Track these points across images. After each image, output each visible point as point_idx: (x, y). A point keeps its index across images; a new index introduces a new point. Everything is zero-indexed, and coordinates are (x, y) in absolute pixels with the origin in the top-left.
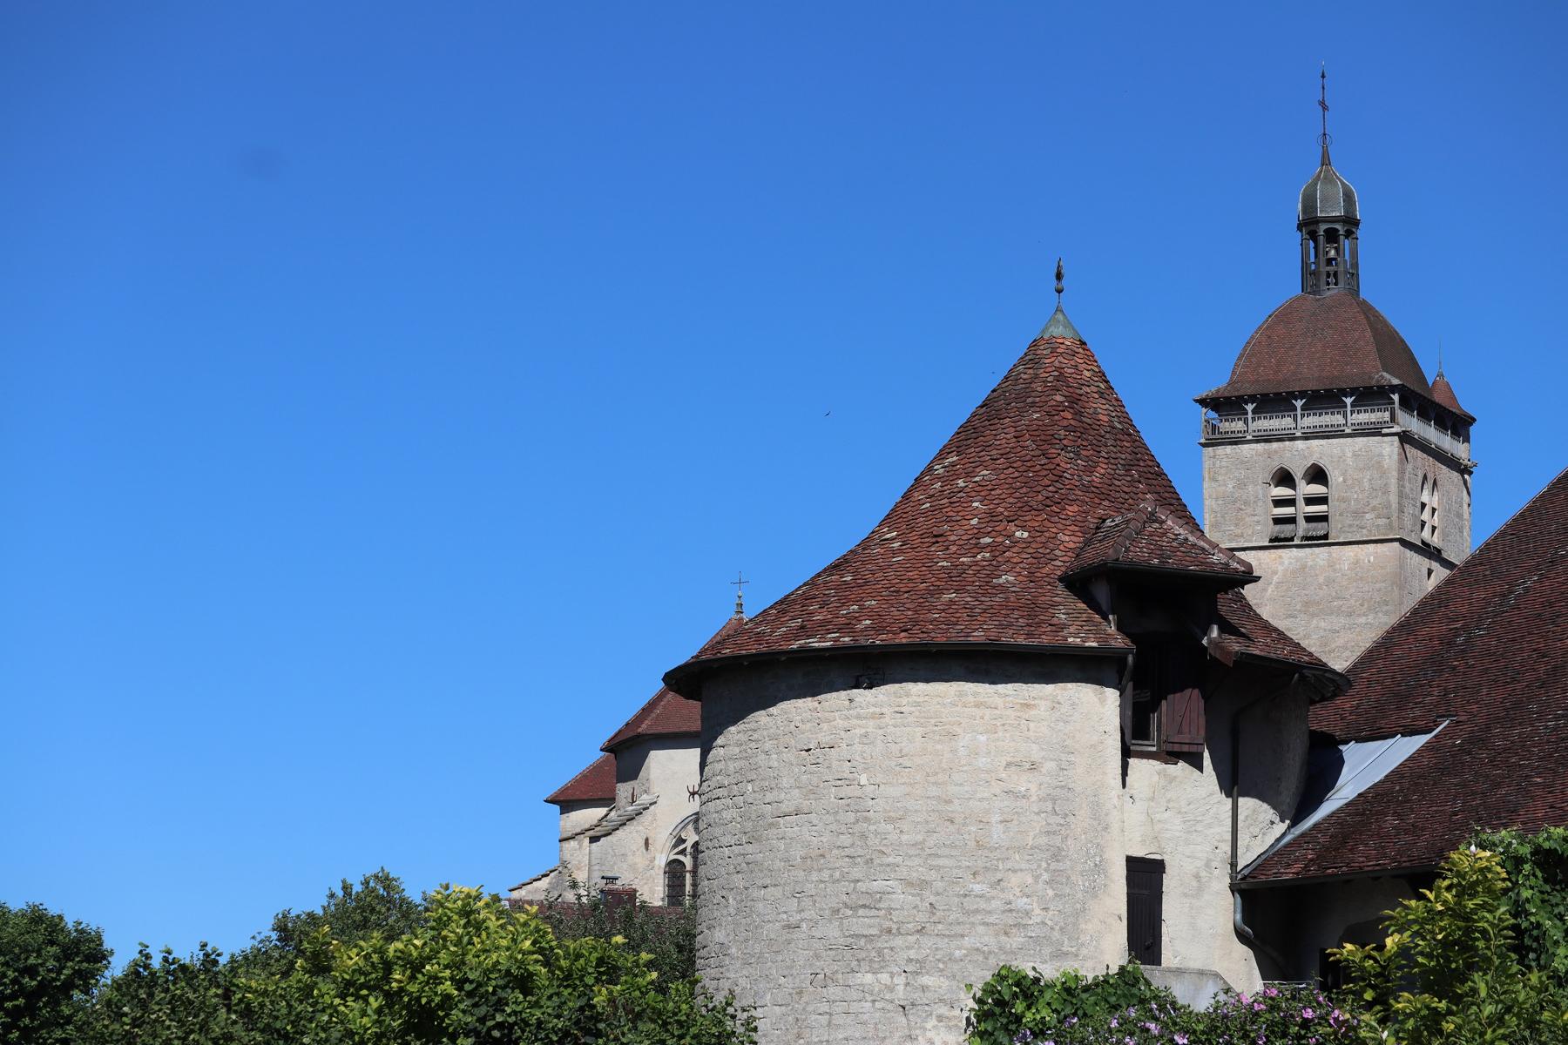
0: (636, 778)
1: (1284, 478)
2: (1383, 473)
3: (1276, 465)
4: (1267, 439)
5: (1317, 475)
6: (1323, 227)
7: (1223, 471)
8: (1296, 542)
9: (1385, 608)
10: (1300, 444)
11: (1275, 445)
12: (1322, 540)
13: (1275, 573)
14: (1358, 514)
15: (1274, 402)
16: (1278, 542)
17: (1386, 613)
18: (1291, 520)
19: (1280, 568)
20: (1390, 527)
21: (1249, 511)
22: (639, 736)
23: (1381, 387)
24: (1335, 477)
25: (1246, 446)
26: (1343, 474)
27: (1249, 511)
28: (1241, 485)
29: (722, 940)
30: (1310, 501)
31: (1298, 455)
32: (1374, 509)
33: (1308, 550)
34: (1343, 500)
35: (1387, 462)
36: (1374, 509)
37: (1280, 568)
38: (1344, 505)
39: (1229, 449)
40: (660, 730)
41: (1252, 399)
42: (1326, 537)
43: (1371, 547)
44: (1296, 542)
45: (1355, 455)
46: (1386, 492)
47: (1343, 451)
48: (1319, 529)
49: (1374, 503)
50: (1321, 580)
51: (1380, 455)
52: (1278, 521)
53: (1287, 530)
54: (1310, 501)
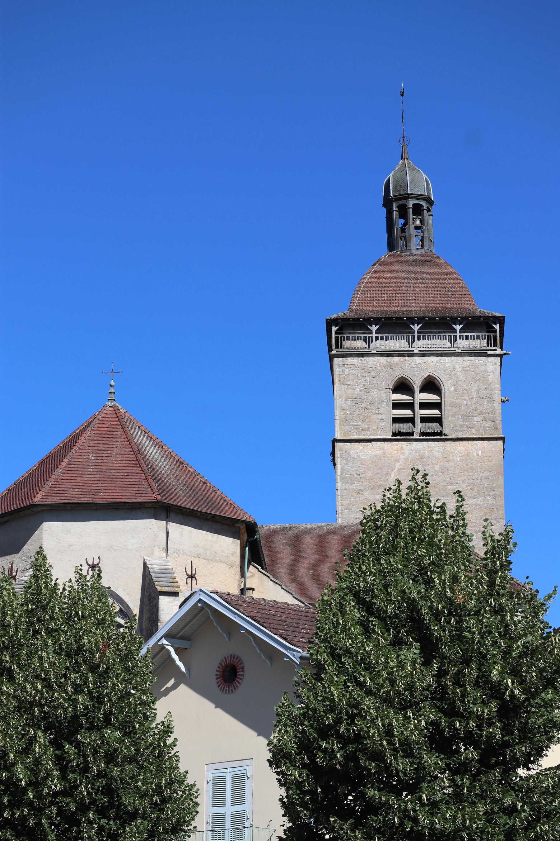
0: (17, 551)
1: (402, 386)
2: (488, 386)
3: (396, 375)
4: (390, 354)
5: (431, 385)
6: (411, 203)
7: (351, 377)
8: (416, 436)
9: (492, 493)
10: (417, 359)
11: (396, 359)
12: (438, 436)
13: (397, 461)
14: (467, 417)
15: (394, 324)
16: (399, 436)
17: (494, 497)
18: (411, 420)
19: (402, 457)
20: (495, 428)
21: (375, 410)
22: (35, 505)
23: (487, 318)
24: (447, 387)
25: (371, 359)
26: (455, 385)
27: (375, 410)
28: (367, 389)
29: (403, 651)
30: (424, 405)
31: (417, 369)
32: (481, 414)
33: (425, 444)
34: (455, 405)
35: (491, 377)
36: (481, 414)
37: (402, 457)
38: (455, 410)
39: (356, 360)
40: (57, 500)
41: (377, 321)
42: (440, 434)
43: (479, 443)
44: (416, 436)
45: (464, 370)
46: (492, 401)
47: (453, 366)
48: (434, 427)
49: (480, 409)
50: (437, 468)
51: (485, 371)
52: (396, 420)
53: (405, 427)
54: (424, 405)
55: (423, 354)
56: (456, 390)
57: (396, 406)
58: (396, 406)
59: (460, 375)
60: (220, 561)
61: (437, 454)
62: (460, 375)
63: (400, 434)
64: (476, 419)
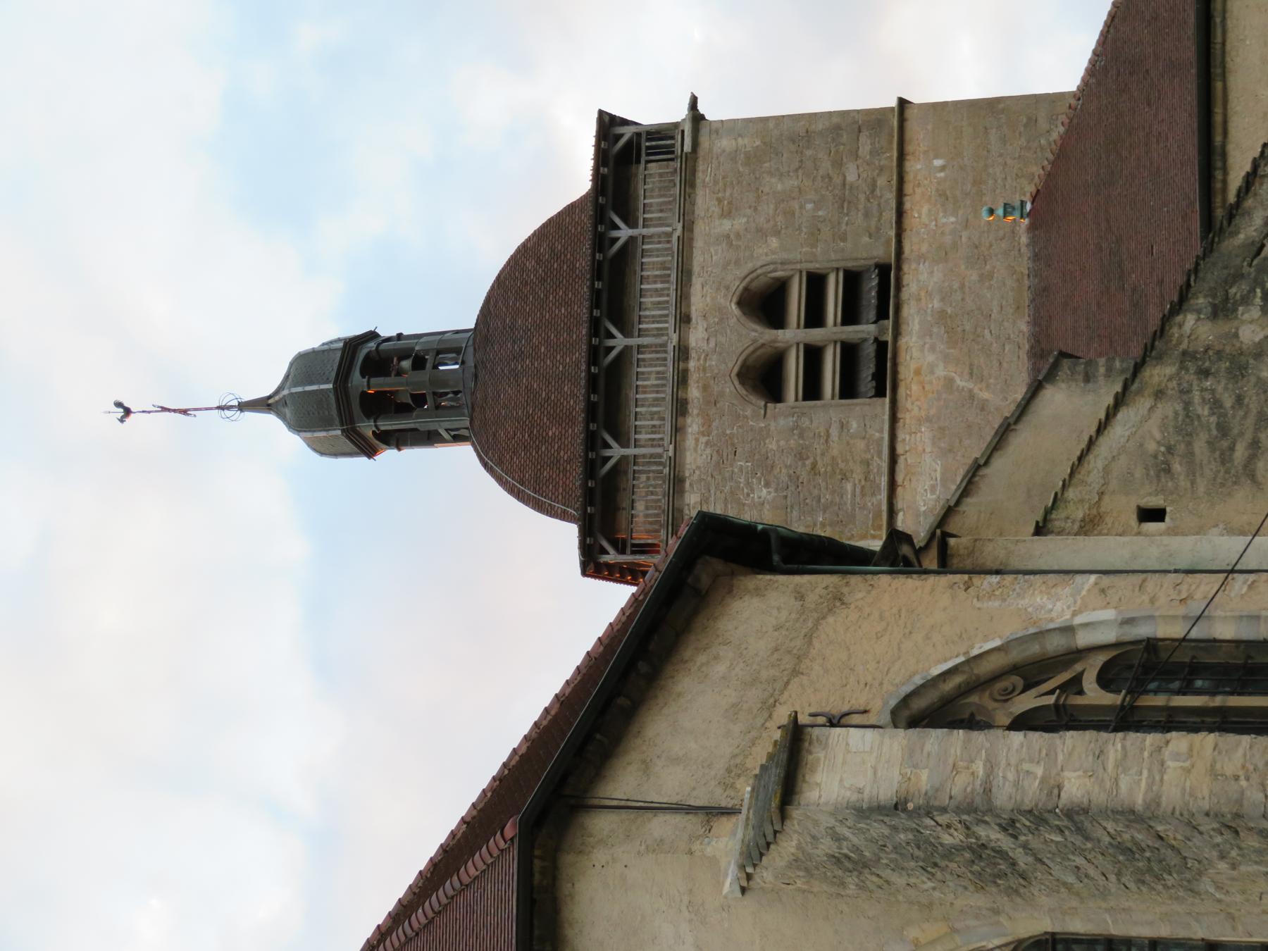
3: (730, 388)
5: (765, 303)
14: (845, 201)
16: (885, 381)
18: (850, 352)
19: (941, 371)
30: (814, 317)
31: (719, 336)
32: (838, 164)
49: (826, 166)
52: (848, 389)
54: (814, 317)
55: (684, 319)
56: (777, 233)
57: (812, 390)
58: (812, 390)
59: (740, 223)
60: (809, 638)
61: (938, 275)
62: (740, 223)
63: (879, 377)
64: (851, 177)
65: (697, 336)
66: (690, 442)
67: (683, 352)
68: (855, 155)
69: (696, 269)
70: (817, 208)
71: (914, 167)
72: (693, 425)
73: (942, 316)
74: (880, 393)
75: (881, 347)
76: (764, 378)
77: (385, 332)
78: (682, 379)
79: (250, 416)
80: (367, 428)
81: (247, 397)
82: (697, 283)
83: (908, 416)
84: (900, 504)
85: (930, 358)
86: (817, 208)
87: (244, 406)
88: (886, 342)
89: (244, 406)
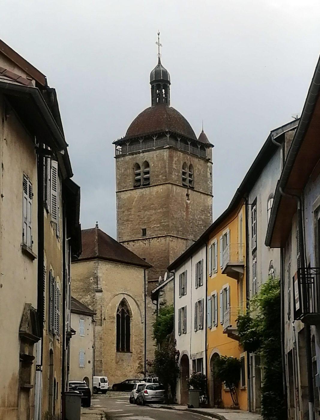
13: (135, 198)
16: (136, 187)
37: (137, 196)
55: (143, 152)
59: (155, 159)
64: (160, 176)
65: (141, 155)
66: (129, 157)
67: (139, 153)
68: (163, 177)
69: (150, 152)
70: (157, 171)
71: (161, 187)
72: (130, 157)
73: (143, 195)
74: (134, 187)
75: (139, 186)
76: (138, 167)
77: (170, 86)
78: (136, 154)
79: (158, 59)
80: (155, 84)
81: (161, 59)
82: (148, 153)
83: (131, 192)
84: (122, 192)
85: (138, 194)
86: (157, 171)
87: (159, 58)
88: (270, 243)
89: (159, 58)
